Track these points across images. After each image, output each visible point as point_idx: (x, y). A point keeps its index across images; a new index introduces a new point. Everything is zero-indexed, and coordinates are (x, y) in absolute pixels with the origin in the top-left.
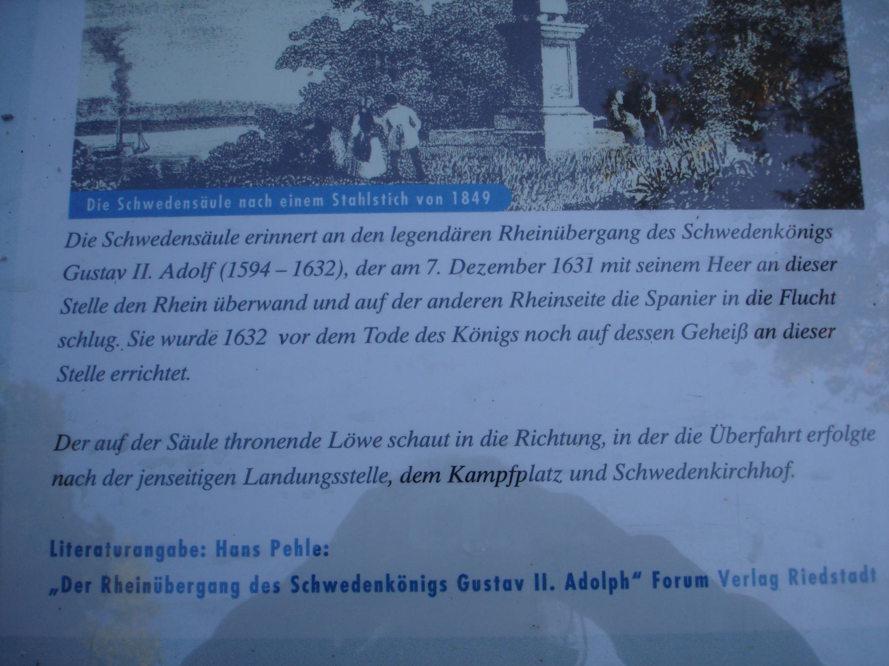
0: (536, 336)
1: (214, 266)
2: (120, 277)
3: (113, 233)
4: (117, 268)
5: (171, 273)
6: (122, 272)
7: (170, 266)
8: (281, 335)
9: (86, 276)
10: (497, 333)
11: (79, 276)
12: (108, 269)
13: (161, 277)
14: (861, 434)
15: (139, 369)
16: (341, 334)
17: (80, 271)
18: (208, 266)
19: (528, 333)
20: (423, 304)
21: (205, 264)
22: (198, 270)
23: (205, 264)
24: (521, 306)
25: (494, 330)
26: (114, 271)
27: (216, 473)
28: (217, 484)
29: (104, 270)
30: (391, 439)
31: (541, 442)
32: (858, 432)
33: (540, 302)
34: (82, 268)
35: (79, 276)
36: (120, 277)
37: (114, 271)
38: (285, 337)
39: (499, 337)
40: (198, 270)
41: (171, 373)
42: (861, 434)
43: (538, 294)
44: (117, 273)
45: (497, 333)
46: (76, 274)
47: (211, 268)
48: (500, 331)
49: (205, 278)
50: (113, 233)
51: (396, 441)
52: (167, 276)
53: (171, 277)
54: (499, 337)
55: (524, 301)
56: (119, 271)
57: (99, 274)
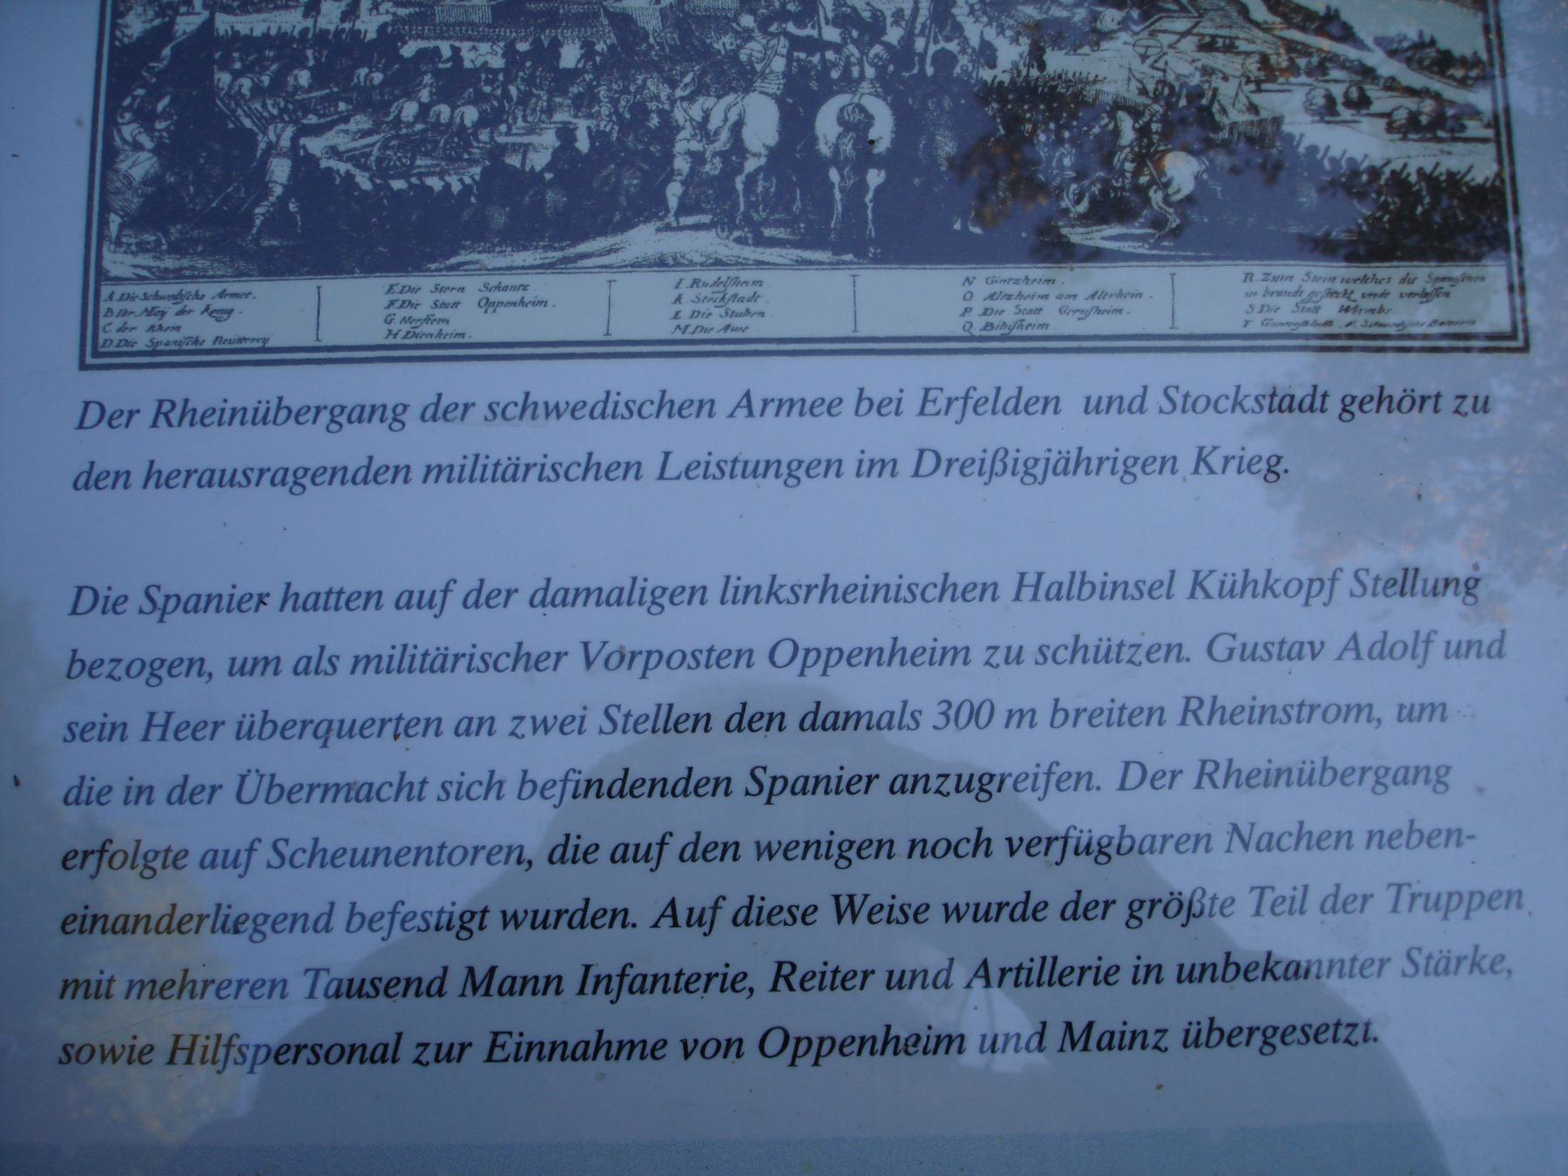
0: (928, 849)
1: (1433, 637)
2: (1314, 656)
3: (287, 841)
4: (1306, 639)
5: (1357, 649)
6: (1317, 646)
7: (1354, 637)
8: (1010, 840)
9: (1249, 654)
10: (830, 843)
11: (1237, 654)
12: (1290, 640)
13: (1339, 658)
14: (478, 918)
15: (722, 970)
16: (880, 841)
17: (1237, 644)
18: (1423, 636)
19: (913, 844)
20: (880, 787)
21: (1417, 633)
22: (1406, 646)
23: (1417, 633)
24: (1214, 785)
25: (824, 838)
26: (1302, 644)
27: (273, 912)
28: (809, 476)
29: (1282, 643)
30: (490, 407)
31: (383, 795)
32: (473, 914)
33: (1248, 778)
34: (1240, 639)
35: (1237, 654)
36: (1314, 656)
37: (1302, 644)
38: (1016, 843)
39: (834, 851)
40: (1406, 646)
41: (683, 979)
42: (478, 918)
43: (1244, 764)
44: (1307, 650)
45: (830, 843)
46: (1232, 650)
47: (1428, 641)
48: (836, 840)
49: (1419, 661)
50: (287, 841)
51: (499, 411)
52: (1350, 655)
53: (1358, 657)
54: (834, 851)
55: (1219, 777)
56: (1311, 644)
57: (1275, 650)
